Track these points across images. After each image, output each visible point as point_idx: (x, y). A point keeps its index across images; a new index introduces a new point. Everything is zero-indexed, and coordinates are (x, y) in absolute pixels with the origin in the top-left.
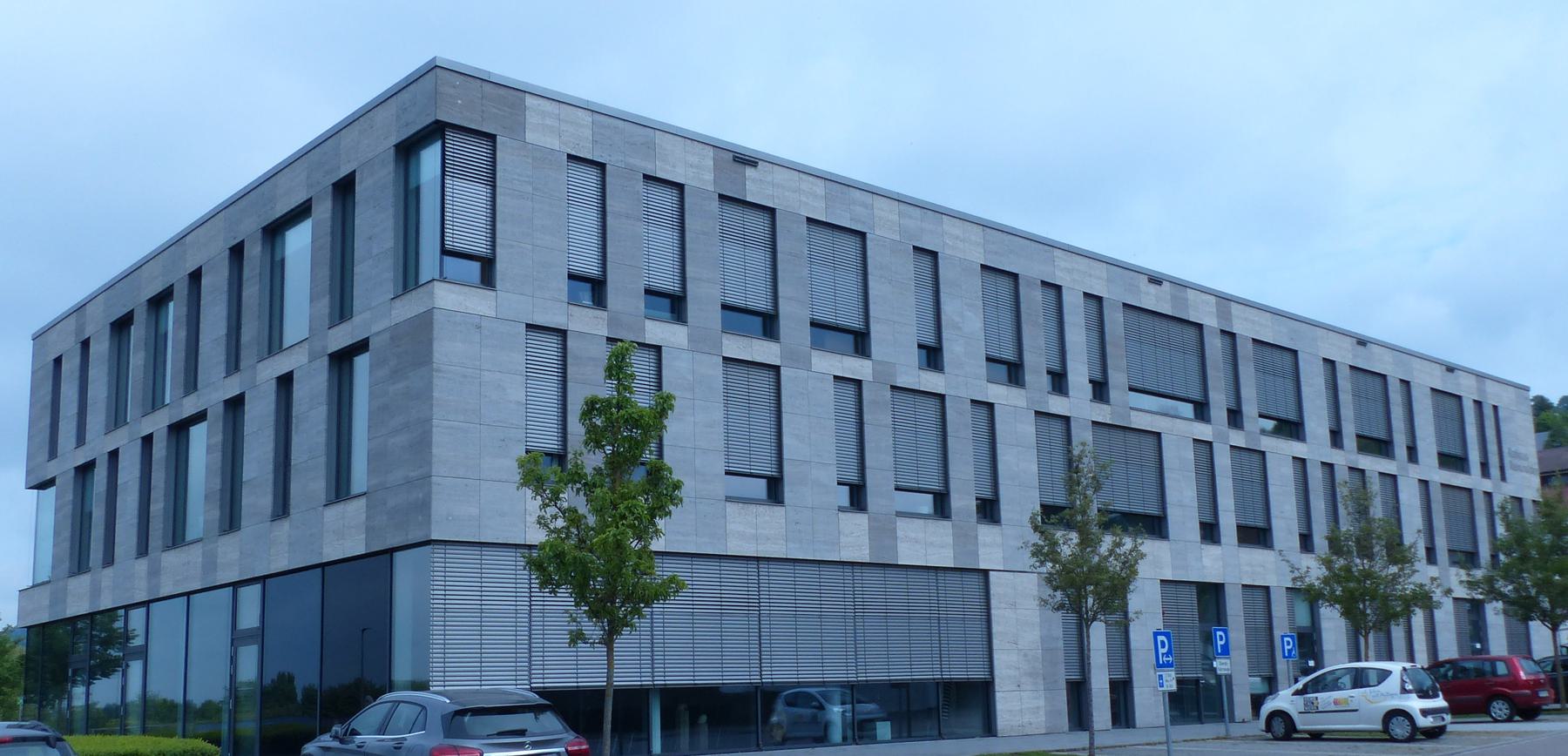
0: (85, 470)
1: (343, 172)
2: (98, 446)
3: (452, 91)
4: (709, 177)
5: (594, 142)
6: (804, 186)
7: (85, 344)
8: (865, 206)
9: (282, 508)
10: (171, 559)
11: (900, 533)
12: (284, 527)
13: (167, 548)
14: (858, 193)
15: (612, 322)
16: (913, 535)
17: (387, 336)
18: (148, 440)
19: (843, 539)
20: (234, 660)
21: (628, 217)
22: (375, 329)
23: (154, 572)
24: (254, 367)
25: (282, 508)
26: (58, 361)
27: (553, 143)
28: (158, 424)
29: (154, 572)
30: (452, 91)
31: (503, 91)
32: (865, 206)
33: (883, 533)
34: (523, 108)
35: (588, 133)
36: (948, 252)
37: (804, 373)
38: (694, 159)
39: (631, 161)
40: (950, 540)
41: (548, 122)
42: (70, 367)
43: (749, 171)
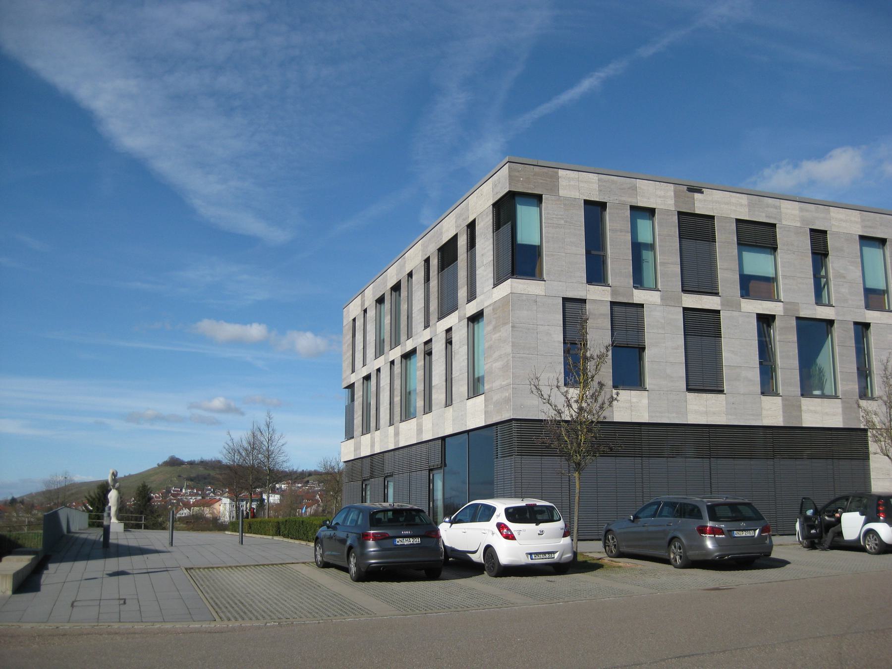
0: (367, 378)
1: (470, 220)
2: (374, 364)
3: (517, 174)
4: (672, 202)
5: (600, 191)
6: (733, 200)
7: (365, 311)
8: (776, 207)
9: (449, 402)
10: (404, 426)
11: (804, 408)
12: (450, 409)
13: (402, 421)
14: (770, 201)
15: (613, 293)
16: (812, 408)
17: (491, 308)
18: (392, 363)
19: (764, 413)
20: (431, 481)
21: (621, 231)
22: (486, 304)
23: (397, 434)
24: (435, 324)
25: (449, 402)
26: (354, 320)
27: (575, 194)
28: (396, 354)
29: (397, 434)
30: (517, 174)
31: (546, 170)
32: (776, 207)
33: (791, 407)
34: (557, 178)
35: (596, 186)
36: (834, 229)
37: (736, 314)
38: (662, 193)
39: (623, 199)
40: (840, 410)
41: (572, 183)
42: (359, 323)
43: (697, 196)
